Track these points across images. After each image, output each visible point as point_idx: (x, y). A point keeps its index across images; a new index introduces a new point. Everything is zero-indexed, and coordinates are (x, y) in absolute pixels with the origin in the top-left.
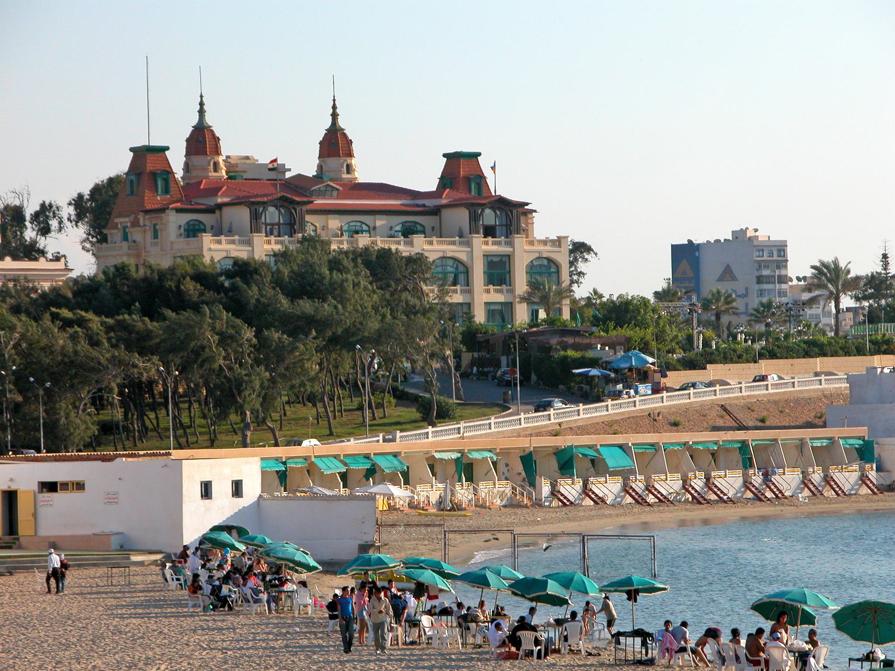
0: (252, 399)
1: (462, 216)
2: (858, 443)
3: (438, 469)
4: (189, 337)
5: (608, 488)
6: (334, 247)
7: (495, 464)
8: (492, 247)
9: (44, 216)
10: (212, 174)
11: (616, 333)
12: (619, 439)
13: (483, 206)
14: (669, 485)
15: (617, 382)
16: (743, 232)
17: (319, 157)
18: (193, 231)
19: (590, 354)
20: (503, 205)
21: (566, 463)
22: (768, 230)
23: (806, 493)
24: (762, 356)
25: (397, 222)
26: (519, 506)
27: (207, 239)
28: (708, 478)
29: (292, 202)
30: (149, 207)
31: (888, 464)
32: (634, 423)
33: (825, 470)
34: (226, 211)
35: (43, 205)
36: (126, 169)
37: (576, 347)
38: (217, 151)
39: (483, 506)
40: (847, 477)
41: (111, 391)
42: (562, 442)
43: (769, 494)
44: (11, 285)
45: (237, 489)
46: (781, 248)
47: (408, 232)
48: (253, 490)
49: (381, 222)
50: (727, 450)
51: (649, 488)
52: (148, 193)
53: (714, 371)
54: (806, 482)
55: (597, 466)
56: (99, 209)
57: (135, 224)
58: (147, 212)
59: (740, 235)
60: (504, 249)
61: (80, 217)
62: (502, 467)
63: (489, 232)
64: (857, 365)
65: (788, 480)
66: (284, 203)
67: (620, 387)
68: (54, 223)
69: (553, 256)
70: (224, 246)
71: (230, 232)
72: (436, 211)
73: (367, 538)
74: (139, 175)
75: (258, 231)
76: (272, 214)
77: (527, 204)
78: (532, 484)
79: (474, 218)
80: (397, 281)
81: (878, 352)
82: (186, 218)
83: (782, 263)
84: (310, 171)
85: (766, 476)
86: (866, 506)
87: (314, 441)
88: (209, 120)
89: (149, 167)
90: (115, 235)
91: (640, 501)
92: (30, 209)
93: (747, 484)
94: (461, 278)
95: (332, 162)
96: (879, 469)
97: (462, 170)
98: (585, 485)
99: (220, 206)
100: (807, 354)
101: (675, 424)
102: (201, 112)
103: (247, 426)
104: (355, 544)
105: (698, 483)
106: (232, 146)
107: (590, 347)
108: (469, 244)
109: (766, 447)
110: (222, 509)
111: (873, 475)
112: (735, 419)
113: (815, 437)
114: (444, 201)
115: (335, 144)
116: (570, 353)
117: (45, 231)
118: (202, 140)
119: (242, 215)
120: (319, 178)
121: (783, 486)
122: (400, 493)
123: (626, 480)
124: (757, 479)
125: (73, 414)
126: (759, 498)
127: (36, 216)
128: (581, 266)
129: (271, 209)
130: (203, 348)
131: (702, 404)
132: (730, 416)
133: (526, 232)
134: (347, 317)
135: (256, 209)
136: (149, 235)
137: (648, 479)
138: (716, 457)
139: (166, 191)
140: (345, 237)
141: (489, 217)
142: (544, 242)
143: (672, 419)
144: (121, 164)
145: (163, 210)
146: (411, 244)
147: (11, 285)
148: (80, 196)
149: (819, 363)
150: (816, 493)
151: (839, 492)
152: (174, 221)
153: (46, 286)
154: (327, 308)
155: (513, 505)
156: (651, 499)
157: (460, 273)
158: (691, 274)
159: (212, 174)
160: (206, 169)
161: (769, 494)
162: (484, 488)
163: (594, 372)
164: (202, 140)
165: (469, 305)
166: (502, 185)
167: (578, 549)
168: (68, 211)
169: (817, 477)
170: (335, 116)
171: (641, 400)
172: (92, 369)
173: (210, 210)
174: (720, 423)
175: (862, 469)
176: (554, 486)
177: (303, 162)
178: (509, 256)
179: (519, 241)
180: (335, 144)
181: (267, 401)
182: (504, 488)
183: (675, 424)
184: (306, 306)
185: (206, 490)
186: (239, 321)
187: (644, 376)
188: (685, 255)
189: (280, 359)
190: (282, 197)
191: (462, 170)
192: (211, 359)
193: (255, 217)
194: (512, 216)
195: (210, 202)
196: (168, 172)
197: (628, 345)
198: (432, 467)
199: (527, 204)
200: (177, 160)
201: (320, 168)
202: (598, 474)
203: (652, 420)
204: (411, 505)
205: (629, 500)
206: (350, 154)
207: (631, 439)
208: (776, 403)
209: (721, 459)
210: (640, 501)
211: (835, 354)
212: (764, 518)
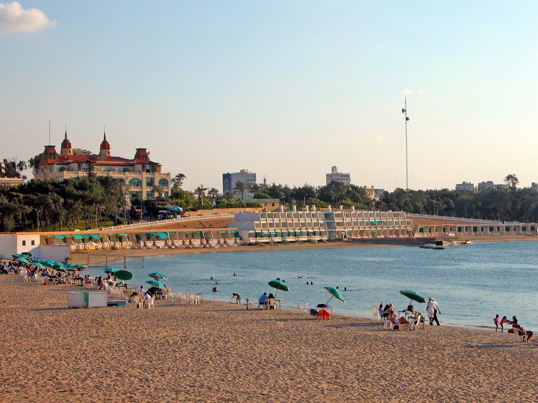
0: (62, 218)
1: (140, 167)
2: (234, 232)
3: (111, 238)
4: (45, 201)
5: (161, 244)
6: (97, 175)
7: (128, 237)
8: (148, 175)
9: (21, 164)
10: (69, 154)
11: (175, 200)
12: (164, 230)
13: (146, 164)
14: (178, 243)
15: (171, 214)
16: (244, 170)
18: (62, 170)
19: (165, 207)
20: (152, 163)
21: (149, 237)
22: (251, 170)
23: (219, 246)
24: (214, 208)
25: (121, 168)
26: (134, 248)
27: (65, 172)
28: (190, 241)
29: (90, 162)
30: (49, 163)
31: (243, 238)
32: (174, 226)
33: (225, 240)
34: (71, 164)
35: (20, 162)
36: (43, 152)
37: (162, 205)
38: (70, 147)
39: (124, 249)
40: (231, 242)
41: (19, 215)
42: (148, 231)
43: (208, 246)
44: (3, 185)
45: (33, 243)
46: (254, 175)
47: (125, 171)
48: (37, 243)
49: (117, 168)
50: (197, 234)
51: (173, 244)
52: (49, 159)
53: (199, 212)
54: (219, 243)
55: (158, 238)
56: (36, 163)
57: (45, 168)
58: (49, 164)
59: (242, 171)
60: (153, 176)
61: (32, 165)
62: (130, 238)
63: (148, 171)
64: (237, 210)
65: (214, 242)
66: (88, 162)
67: (172, 216)
68: (24, 167)
69: (166, 178)
70: (70, 174)
71: (73, 170)
72: (133, 165)
73: (68, 256)
74: (47, 154)
75: (80, 170)
76: (84, 166)
78: (138, 243)
79: (143, 168)
80: (110, 186)
81: (248, 207)
82: (59, 166)
83: (255, 180)
84: (97, 153)
85: (207, 241)
86: (237, 250)
87: (78, 230)
88: (68, 138)
89: (50, 152)
90: (40, 171)
91: (170, 248)
92: (17, 163)
93: (202, 243)
94: (140, 184)
95: (104, 151)
96: (241, 239)
97: (141, 154)
98: (154, 243)
99: (69, 163)
100: (227, 207)
101: (185, 227)
102: (66, 136)
103: (61, 226)
104: (64, 258)
105: (187, 243)
106: (75, 146)
107: (166, 204)
108: (142, 175)
109: (208, 233)
110: (28, 248)
111: (238, 241)
112: (203, 225)
113: (222, 230)
114: (135, 162)
115: (105, 146)
116: (160, 206)
117: (21, 169)
118: (66, 144)
119: (76, 166)
120: (100, 155)
121: (212, 244)
122: (100, 245)
123: (166, 242)
124: (205, 242)
125: (8, 222)
126: (205, 247)
127: (19, 165)
128: (182, 181)
129: (84, 164)
130: (48, 204)
131: (194, 221)
132: (201, 224)
133: (159, 171)
134: (92, 195)
135: (79, 164)
136: (49, 171)
137: (172, 242)
138: (193, 235)
139: (54, 158)
140: (106, 172)
141: (148, 167)
142: (164, 174)
143: (184, 225)
144: (42, 151)
145: (53, 164)
146: (125, 174)
147: (3, 185)
148: (32, 159)
149: (231, 210)
150: (222, 246)
151: (228, 245)
152: (56, 167)
153: (13, 185)
154: (87, 193)
155: (133, 248)
156: (173, 247)
157: (139, 183)
158: (228, 182)
159: (69, 154)
160: (67, 152)
161: (208, 246)
162: (124, 243)
163: (165, 212)
164: (66, 144)
166: (152, 158)
167: (90, 263)
168: (28, 164)
169: (222, 241)
170: (105, 137)
171: (179, 219)
172: (13, 210)
173: (67, 164)
174: (199, 226)
175: (235, 239)
176: (145, 243)
177: (96, 151)
179: (156, 174)
180: (105, 146)
181: (67, 219)
182: (130, 243)
183: (185, 227)
184: (81, 192)
185: (24, 243)
186: (59, 197)
187: (179, 213)
188: (227, 177)
189: (71, 207)
190: (89, 160)
191: (141, 154)
192: (50, 207)
193: (79, 166)
194: (155, 167)
195: (67, 162)
196: (55, 153)
197: (177, 204)
198: (109, 238)
200: (58, 150)
201: (100, 152)
202: (158, 240)
203: (179, 225)
204: (102, 248)
205: (167, 247)
206: (109, 149)
207: (168, 231)
209: (195, 236)
210: (170, 248)
211: (235, 207)
212: (206, 253)
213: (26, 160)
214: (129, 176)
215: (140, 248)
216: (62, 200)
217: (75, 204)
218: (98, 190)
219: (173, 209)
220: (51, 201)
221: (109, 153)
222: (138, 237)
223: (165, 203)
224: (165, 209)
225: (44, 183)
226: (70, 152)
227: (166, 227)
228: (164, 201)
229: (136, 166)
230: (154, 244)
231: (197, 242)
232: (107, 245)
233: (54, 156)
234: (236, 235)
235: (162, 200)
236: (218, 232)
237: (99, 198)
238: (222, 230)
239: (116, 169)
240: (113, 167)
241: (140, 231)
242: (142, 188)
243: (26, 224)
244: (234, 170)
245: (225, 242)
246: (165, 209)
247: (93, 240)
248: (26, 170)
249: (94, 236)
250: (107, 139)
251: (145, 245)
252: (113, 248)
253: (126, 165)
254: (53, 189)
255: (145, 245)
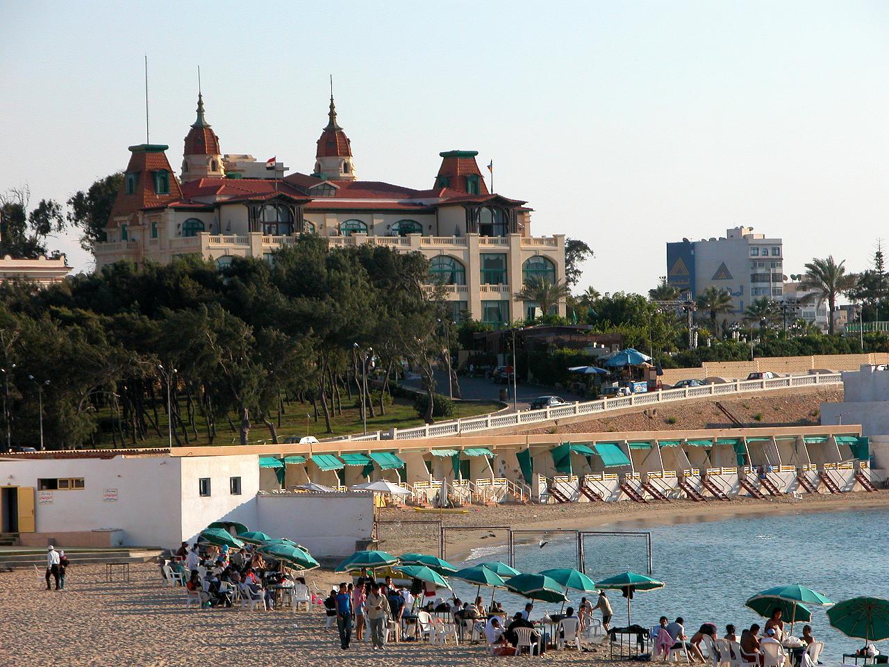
0: (250, 397)
1: (458, 215)
3: (435, 467)
5: (605, 485)
7: (491, 461)
9: (44, 214)
10: (211, 173)
12: (615, 436)
13: (480, 205)
14: (664, 482)
17: (317, 156)
18: (192, 229)
19: (586, 352)
21: (562, 460)
22: (763, 230)
24: (757, 354)
26: (516, 503)
28: (703, 476)
29: (291, 201)
30: (147, 205)
33: (820, 467)
34: (224, 209)
37: (572, 345)
38: (216, 150)
42: (559, 439)
43: (764, 491)
44: (11, 283)
45: (236, 486)
46: (775, 247)
47: (405, 231)
48: (251, 487)
49: (378, 221)
51: (645, 485)
52: (147, 193)
53: (709, 369)
54: (800, 479)
55: (593, 463)
56: (100, 207)
57: (134, 222)
58: (146, 210)
59: (734, 234)
62: (498, 464)
63: (486, 230)
64: (851, 363)
65: (782, 477)
67: (615, 384)
68: (53, 222)
69: (549, 254)
70: (223, 245)
71: (229, 231)
72: (433, 210)
73: (365, 535)
76: (270, 213)
77: (524, 203)
78: (529, 482)
79: (471, 217)
80: (395, 280)
82: (183, 217)
83: (777, 262)
84: (308, 169)
87: (312, 439)
88: (208, 119)
92: (30, 208)
93: (742, 481)
94: (458, 276)
95: (330, 161)
97: (458, 170)
99: (219, 205)
100: (802, 353)
101: (671, 422)
102: (200, 111)
103: (245, 424)
105: (694, 481)
108: (466, 242)
109: (760, 445)
110: (221, 505)
111: (867, 472)
112: (731, 417)
113: (810, 435)
115: (333, 143)
116: (566, 351)
117: (45, 229)
118: (200, 140)
124: (752, 477)
125: (72, 412)
126: (754, 495)
127: (36, 215)
128: (577, 265)
129: (270, 208)
130: (202, 346)
131: (697, 402)
132: (724, 414)
135: (255, 208)
136: (148, 234)
137: (643, 477)
138: (711, 454)
139: (165, 189)
141: (486, 216)
142: (541, 241)
144: (119, 163)
145: (161, 209)
147: (11, 283)
148: (80, 195)
149: (813, 361)
150: (810, 491)
151: (834, 489)
152: (173, 220)
155: (509, 502)
156: (647, 496)
159: (211, 173)
161: (764, 491)
162: (481, 485)
164: (200, 140)
165: (466, 303)
166: (500, 184)
168: (67, 210)
169: (811, 474)
170: (332, 115)
171: (637, 398)
174: (715, 420)
175: (856, 467)
177: (301, 160)
178: (505, 254)
180: (333, 143)
183: (671, 422)
184: (304, 304)
186: (237, 319)
187: (639, 374)
188: (680, 254)
190: (280, 196)
191: (458, 170)
193: (254, 215)
194: (507, 215)
195: (209, 200)
196: (167, 171)
198: (429, 465)
199: (524, 203)
200: (176, 159)
201: (318, 166)
203: (648, 418)
205: (625, 497)
206: (348, 153)
208: (770, 400)
210: (636, 498)
211: (829, 352)
212: (759, 515)
213: (62, 198)
214: (426, 246)
215: (535, 501)
216: (247, 332)
217: (293, 347)
218: (360, 293)
219: (620, 363)
220: (212, 337)
221: (347, 168)
222: (525, 458)
223: (582, 339)
224: (589, 361)
225: (161, 273)
226: (215, 164)
227: (606, 424)
228: (571, 331)
229: (443, 212)
230: (582, 488)
231: (725, 479)
232: (428, 489)
233: (165, 180)
234: (859, 450)
235: (561, 329)
236: (796, 442)
237: (371, 323)
238: (810, 435)
239: (376, 222)
240: (365, 218)
241: (535, 439)
242: (467, 290)
243: (220, 412)
244: (704, 228)
245: (822, 477)
246: (589, 361)
247: (449, 466)
248: (61, 235)
249: (380, 460)
250: (339, 122)
251: (551, 490)
252: (446, 504)
253: (414, 210)
254: (200, 292)
255: (551, 490)
